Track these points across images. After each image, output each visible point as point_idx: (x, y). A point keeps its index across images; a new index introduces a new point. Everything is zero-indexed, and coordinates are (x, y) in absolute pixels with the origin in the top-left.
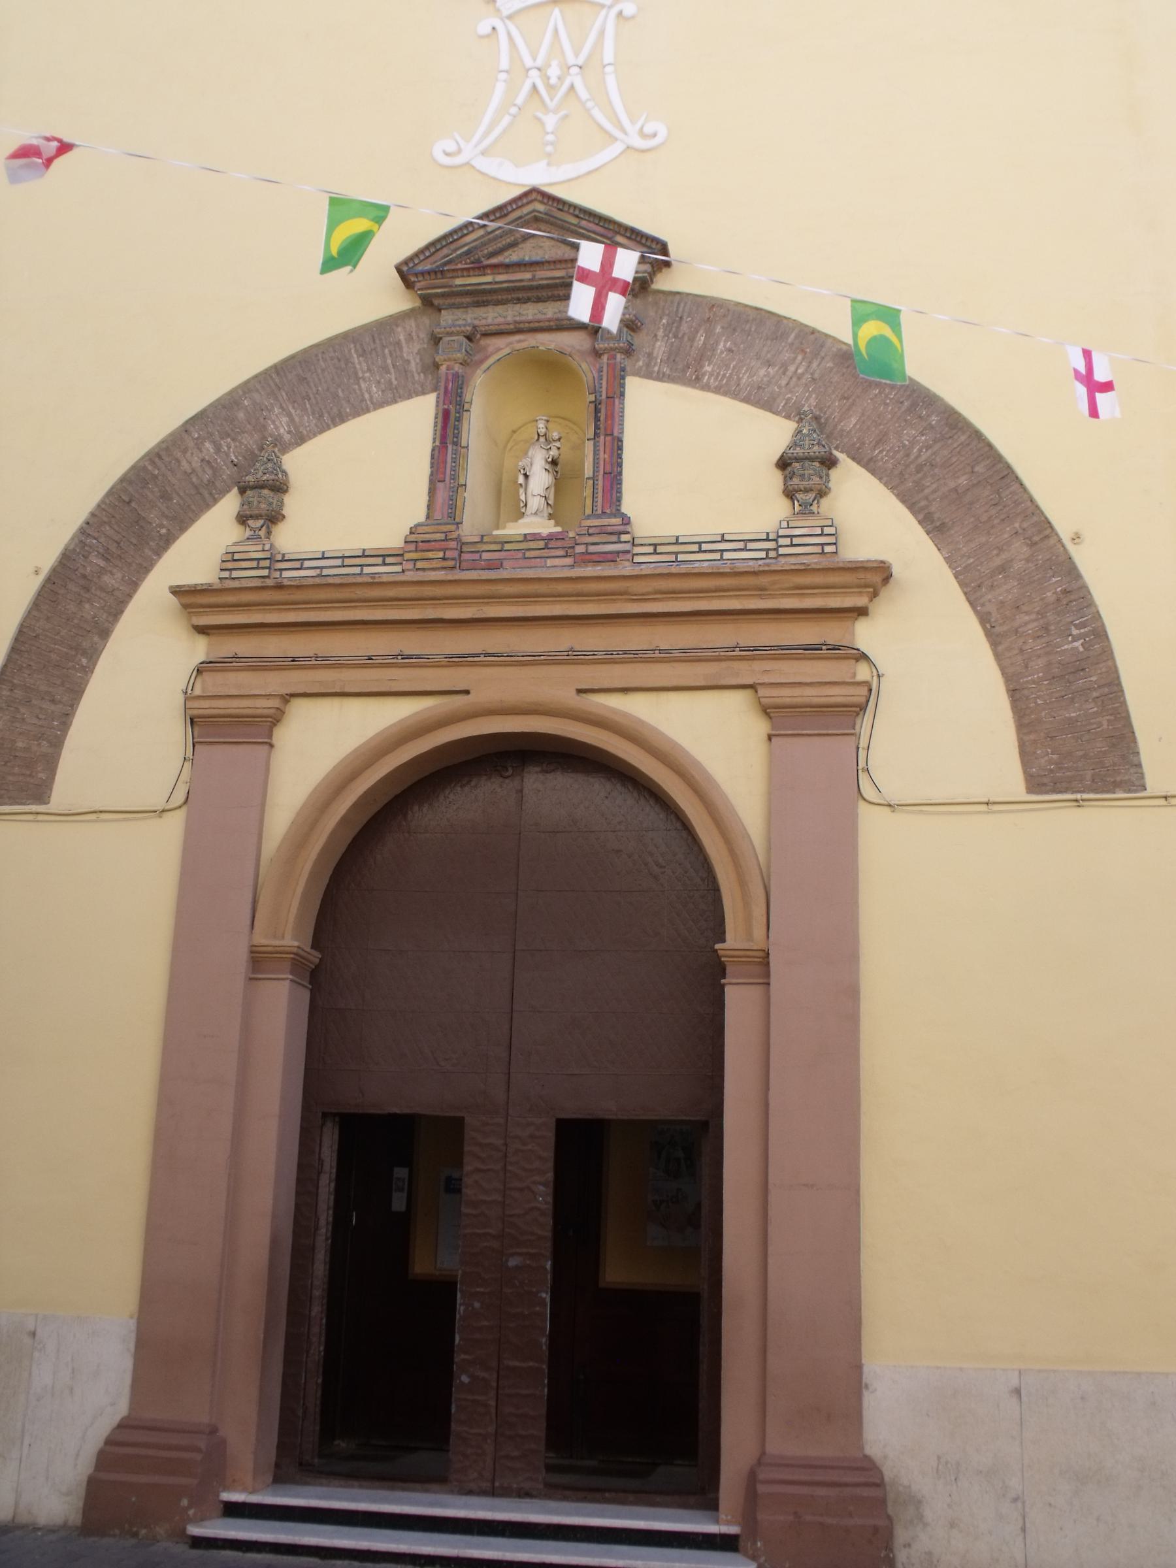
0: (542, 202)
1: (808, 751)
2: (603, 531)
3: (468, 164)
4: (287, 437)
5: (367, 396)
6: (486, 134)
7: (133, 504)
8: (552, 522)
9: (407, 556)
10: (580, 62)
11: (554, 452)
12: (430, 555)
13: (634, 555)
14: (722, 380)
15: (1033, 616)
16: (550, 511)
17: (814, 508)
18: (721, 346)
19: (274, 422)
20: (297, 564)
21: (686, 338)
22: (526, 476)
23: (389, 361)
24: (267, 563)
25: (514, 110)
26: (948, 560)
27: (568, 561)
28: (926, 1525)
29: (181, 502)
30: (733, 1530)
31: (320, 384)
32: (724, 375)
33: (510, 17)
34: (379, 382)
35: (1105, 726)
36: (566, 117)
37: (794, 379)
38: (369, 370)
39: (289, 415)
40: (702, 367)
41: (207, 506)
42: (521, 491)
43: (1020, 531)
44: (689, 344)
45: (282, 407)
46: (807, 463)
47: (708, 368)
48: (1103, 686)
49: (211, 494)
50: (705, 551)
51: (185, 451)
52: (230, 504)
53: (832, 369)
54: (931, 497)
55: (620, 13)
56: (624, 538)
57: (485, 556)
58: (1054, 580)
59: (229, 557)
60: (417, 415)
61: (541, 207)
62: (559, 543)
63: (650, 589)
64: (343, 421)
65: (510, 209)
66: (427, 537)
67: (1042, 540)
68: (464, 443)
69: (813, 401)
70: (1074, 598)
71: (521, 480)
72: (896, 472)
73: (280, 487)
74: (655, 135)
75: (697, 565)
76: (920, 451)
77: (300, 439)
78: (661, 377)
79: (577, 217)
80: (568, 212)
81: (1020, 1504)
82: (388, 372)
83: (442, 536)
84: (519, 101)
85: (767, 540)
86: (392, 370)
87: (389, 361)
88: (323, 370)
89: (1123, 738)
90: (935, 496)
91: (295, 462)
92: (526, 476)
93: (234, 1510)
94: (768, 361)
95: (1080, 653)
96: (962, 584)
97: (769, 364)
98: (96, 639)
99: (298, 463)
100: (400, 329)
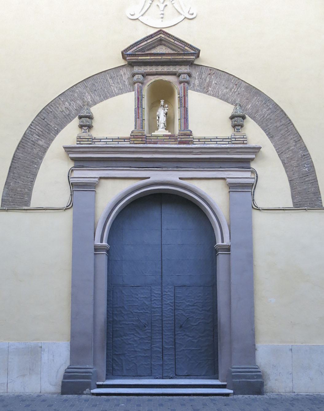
1: (242, 196)
2: (185, 135)
3: (137, 19)
5: (114, 91)
7: (45, 120)
8: (168, 131)
11: (166, 111)
13: (194, 142)
14: (214, 92)
15: (295, 161)
16: (165, 128)
17: (240, 130)
18: (213, 82)
19: (86, 97)
21: (204, 79)
22: (159, 117)
23: (119, 81)
26: (275, 146)
28: (270, 380)
29: (60, 120)
30: (225, 383)
31: (97, 86)
32: (215, 91)
34: (117, 87)
35: (313, 190)
36: (166, 6)
37: (234, 93)
38: (113, 83)
39: (91, 96)
40: (208, 88)
42: (158, 121)
43: (293, 138)
45: (88, 93)
46: (239, 118)
47: (210, 89)
48: (313, 180)
49: (69, 118)
50: (212, 141)
51: (60, 104)
52: (76, 122)
53: (244, 91)
54: (270, 128)
56: (191, 137)
58: (301, 152)
59: (79, 138)
61: (163, 36)
64: (107, 99)
65: (154, 36)
66: (137, 134)
67: (298, 141)
68: (143, 107)
69: (239, 100)
72: (261, 121)
74: (193, 14)
76: (267, 115)
77: (95, 103)
78: (197, 91)
79: (174, 40)
81: (291, 375)
82: (119, 84)
83: (141, 134)
86: (120, 84)
88: (99, 82)
90: (271, 128)
91: (95, 110)
92: (159, 117)
93: (99, 386)
94: (226, 87)
95: (307, 171)
96: (277, 152)
97: (227, 88)
98: (38, 160)
100: (121, 71)
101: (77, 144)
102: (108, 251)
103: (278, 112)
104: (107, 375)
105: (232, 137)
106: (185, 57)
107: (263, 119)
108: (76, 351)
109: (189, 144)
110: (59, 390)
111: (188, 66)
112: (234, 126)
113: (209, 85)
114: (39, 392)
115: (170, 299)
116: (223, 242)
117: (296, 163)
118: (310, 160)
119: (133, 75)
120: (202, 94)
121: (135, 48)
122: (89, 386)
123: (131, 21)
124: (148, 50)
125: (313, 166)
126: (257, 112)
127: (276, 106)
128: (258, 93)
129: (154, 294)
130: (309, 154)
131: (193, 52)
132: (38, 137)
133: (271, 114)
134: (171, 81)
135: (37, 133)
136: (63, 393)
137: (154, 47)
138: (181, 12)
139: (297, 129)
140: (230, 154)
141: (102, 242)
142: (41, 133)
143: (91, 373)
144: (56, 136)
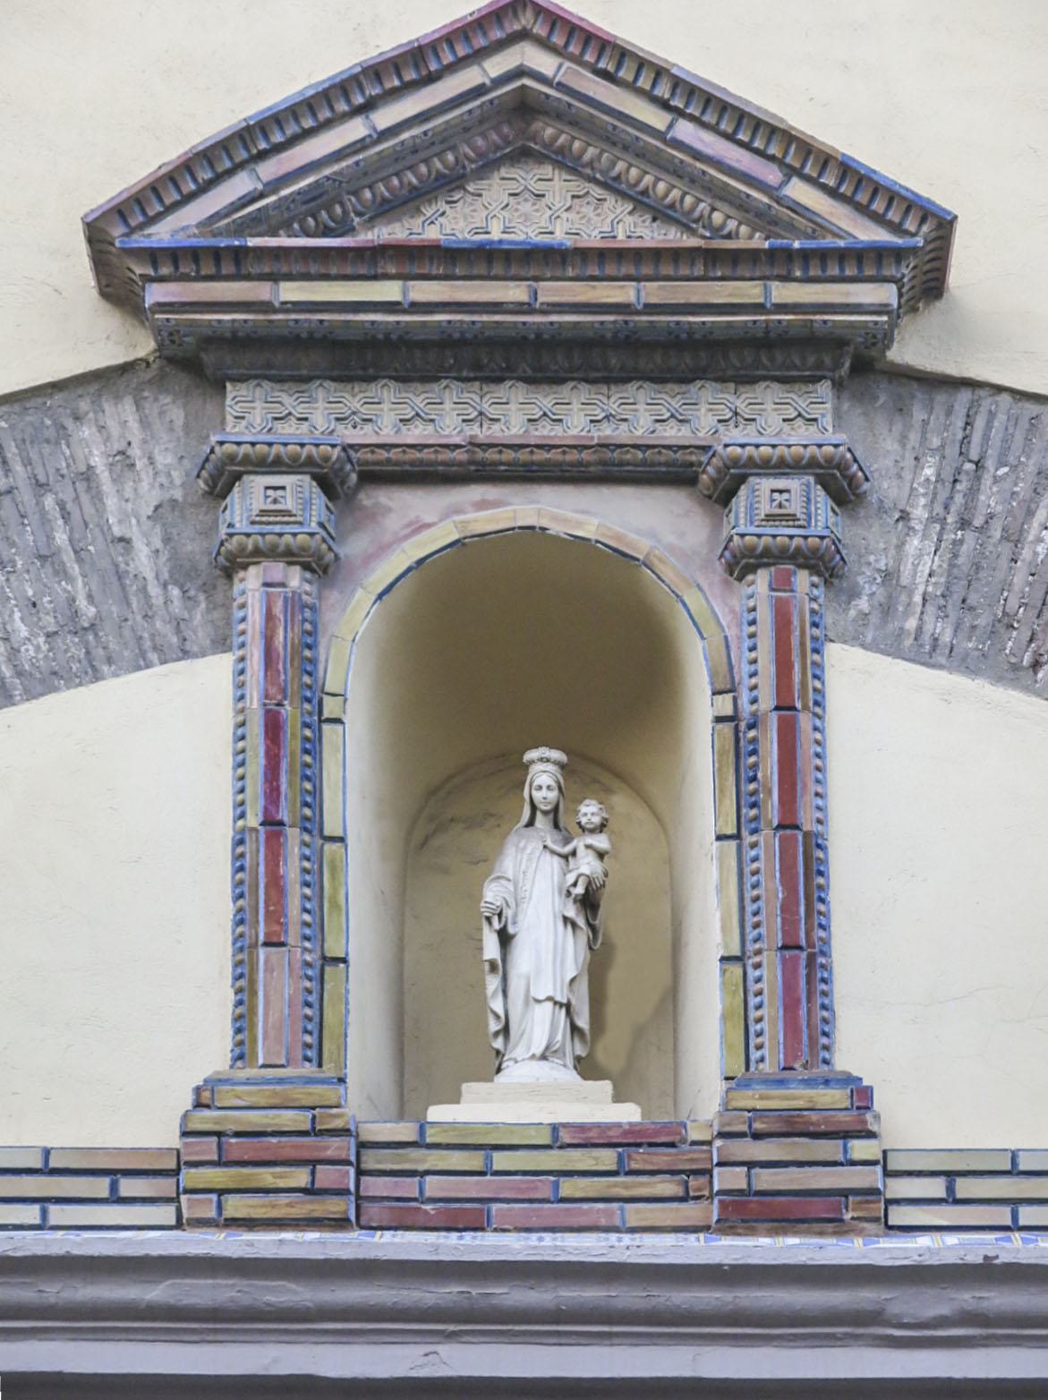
0: (545, 44)
2: (793, 1126)
9: (189, 1177)
11: (587, 865)
12: (267, 1176)
13: (889, 1202)
16: (581, 1050)
22: (505, 938)
23: (61, 538)
42: (493, 983)
44: (1006, 550)
56: (860, 1149)
57: (433, 1186)
61: (544, 63)
62: (662, 1158)
63: (944, 1310)
66: (256, 1119)
71: (491, 949)
75: (924, 1241)
78: (926, 653)
79: (665, 105)
80: (631, 87)
82: (62, 573)
83: (300, 1120)
86: (75, 569)
87: (61, 538)
92: (505, 938)
100: (87, 432)
109: (834, 1224)
111: (824, 389)
119: (221, 479)
121: (242, 184)
131: (869, 233)
134: (640, 546)
137: (450, 183)
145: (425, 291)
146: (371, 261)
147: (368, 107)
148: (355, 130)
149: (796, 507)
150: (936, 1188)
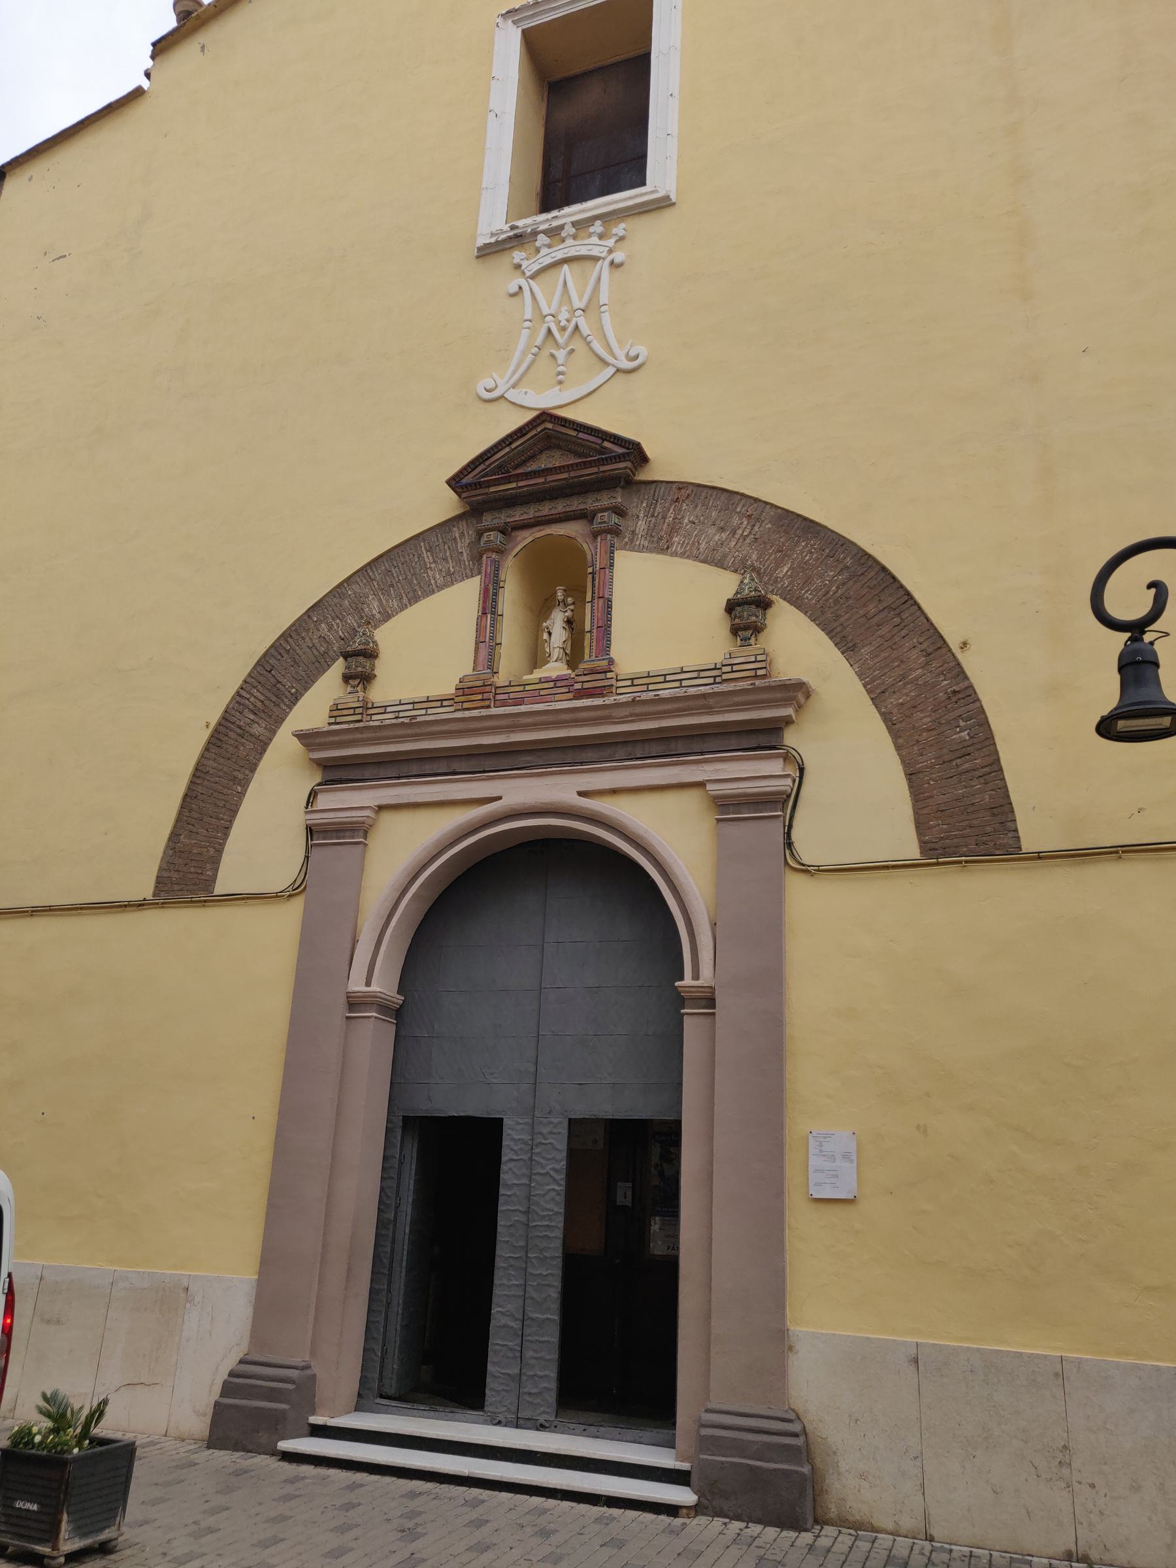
0: (550, 422)
3: (502, 397)
4: (378, 616)
6: (514, 372)
9: (457, 699)
10: (582, 306)
11: (569, 614)
12: (473, 697)
17: (752, 641)
20: (382, 710)
24: (360, 710)
25: (535, 350)
26: (860, 675)
27: (570, 695)
30: (685, 1466)
31: (399, 574)
33: (533, 277)
36: (572, 351)
38: (435, 562)
39: (380, 600)
40: (672, 538)
41: (322, 671)
46: (746, 607)
51: (308, 631)
52: (338, 667)
55: (612, 263)
56: (609, 675)
60: (464, 596)
61: (550, 426)
62: (564, 683)
66: (470, 684)
69: (754, 557)
70: (964, 697)
71: (545, 636)
73: (371, 654)
74: (637, 357)
76: (838, 588)
77: (387, 617)
83: (481, 683)
84: (538, 342)
85: (715, 669)
89: (1003, 809)
92: (550, 634)
96: (869, 692)
97: (722, 529)
98: (247, 772)
99: (385, 636)
101: (330, 724)
102: (398, 1014)
103: (872, 574)
104: (359, 1395)
105: (726, 662)
106: (603, 468)
107: (827, 600)
108: (269, 1304)
109: (602, 695)
110: (200, 1426)
111: (619, 489)
112: (735, 631)
113: (673, 530)
114: (164, 1432)
115: (553, 1159)
116: (696, 976)
117: (929, 719)
118: (978, 704)
119: (480, 534)
120: (654, 555)
121: (482, 467)
122: (278, 1425)
123: (487, 405)
124: (517, 467)
125: (985, 723)
126: (808, 581)
127: (865, 558)
128: (810, 527)
129: (512, 1143)
130: (971, 686)
131: (620, 450)
132: (252, 717)
133: (851, 583)
134: (573, 534)
135: (251, 707)
136: (214, 1442)
137: (532, 457)
138: (609, 359)
139: (930, 616)
140: (718, 712)
141: (368, 984)
142: (259, 704)
143: (293, 1382)
144: (291, 709)
145: (521, 484)
146: (518, 477)
147: (511, 444)
148: (507, 449)
149: (606, 519)
150: (629, 683)
